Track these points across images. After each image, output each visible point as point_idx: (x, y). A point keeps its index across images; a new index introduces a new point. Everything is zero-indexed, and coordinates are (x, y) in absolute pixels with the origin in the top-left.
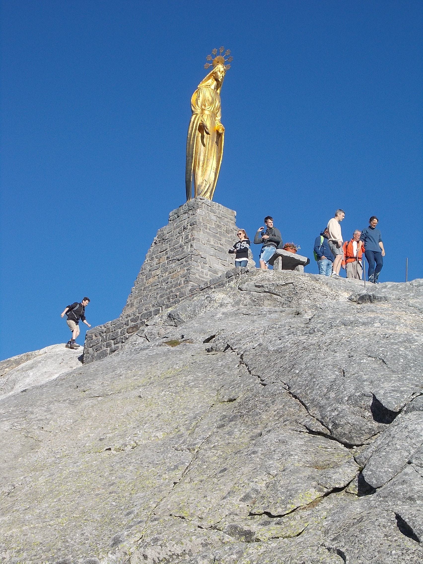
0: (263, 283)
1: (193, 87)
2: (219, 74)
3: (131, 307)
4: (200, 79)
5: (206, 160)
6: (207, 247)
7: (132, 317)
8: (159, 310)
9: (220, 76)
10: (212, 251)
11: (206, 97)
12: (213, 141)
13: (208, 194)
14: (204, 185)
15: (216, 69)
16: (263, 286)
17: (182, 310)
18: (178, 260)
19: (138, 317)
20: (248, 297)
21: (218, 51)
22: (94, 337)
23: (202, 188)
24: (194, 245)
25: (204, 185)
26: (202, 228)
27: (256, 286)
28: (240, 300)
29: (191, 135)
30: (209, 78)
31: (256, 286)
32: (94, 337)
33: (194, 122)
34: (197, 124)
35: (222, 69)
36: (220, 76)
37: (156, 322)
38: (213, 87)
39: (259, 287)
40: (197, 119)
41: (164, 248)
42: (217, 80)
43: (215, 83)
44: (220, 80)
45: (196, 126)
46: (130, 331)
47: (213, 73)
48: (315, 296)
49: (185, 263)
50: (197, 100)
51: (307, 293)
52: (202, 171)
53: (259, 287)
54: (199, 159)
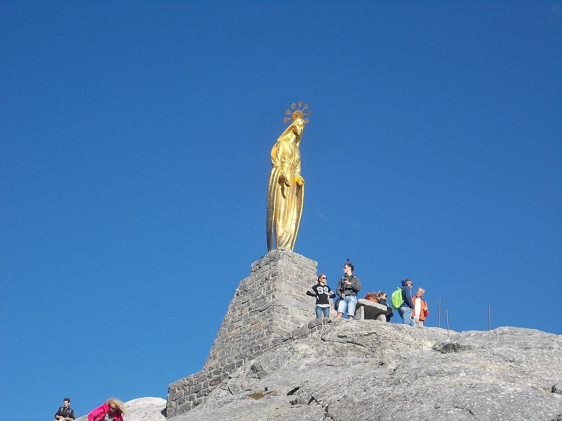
0: (346, 333)
1: (273, 141)
2: (298, 127)
3: (214, 359)
4: (279, 133)
5: (287, 212)
6: (289, 298)
7: (215, 369)
8: (242, 362)
9: (299, 129)
10: (294, 302)
11: (286, 151)
12: (293, 192)
13: (289, 245)
14: (285, 236)
15: (295, 123)
16: (346, 336)
17: (265, 362)
18: (261, 311)
19: (221, 369)
20: (331, 347)
21: (297, 105)
22: (177, 390)
23: (283, 239)
24: (276, 296)
25: (285, 236)
26: (283, 279)
27: (339, 336)
28: (323, 351)
29: (271, 188)
30: (288, 132)
31: (339, 336)
32: (177, 390)
33: (274, 175)
34: (277, 177)
35: (301, 123)
36: (299, 129)
37: (239, 375)
38: (292, 140)
39: (342, 337)
40: (277, 171)
41: (246, 300)
42: (296, 133)
43: (294, 136)
44: (299, 133)
45: (276, 179)
46: (213, 383)
47: (292, 127)
48: (399, 345)
49: (267, 314)
50: (277, 153)
51: (390, 343)
52: (283, 223)
53: (342, 337)
54: (280, 211)
